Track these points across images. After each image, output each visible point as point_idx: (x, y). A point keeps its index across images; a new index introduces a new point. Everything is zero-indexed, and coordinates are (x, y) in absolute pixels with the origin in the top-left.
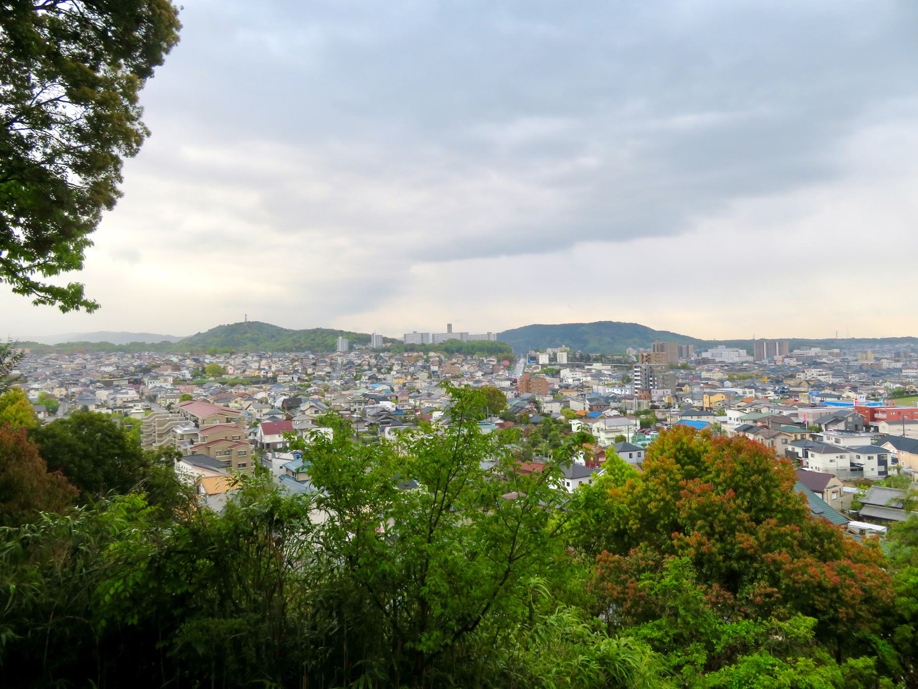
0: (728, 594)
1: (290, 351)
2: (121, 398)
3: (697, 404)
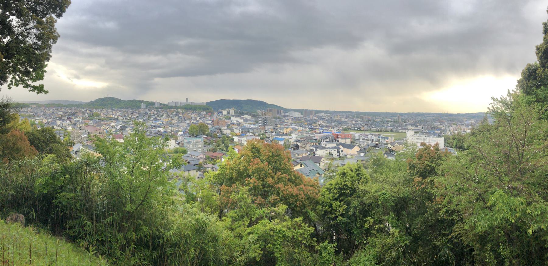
0: (263, 200)
1: (123, 108)
2: (64, 124)
3: (282, 131)
